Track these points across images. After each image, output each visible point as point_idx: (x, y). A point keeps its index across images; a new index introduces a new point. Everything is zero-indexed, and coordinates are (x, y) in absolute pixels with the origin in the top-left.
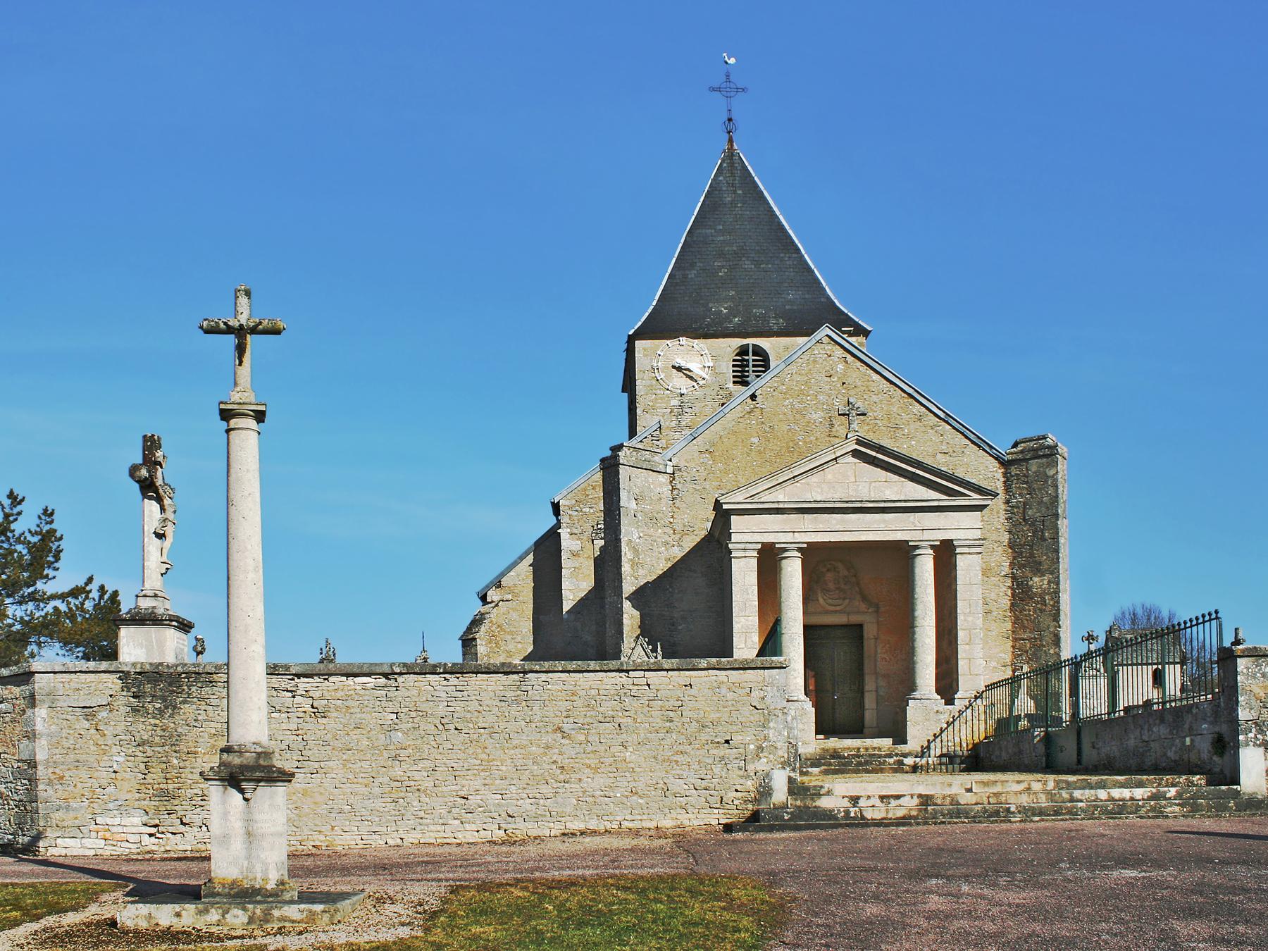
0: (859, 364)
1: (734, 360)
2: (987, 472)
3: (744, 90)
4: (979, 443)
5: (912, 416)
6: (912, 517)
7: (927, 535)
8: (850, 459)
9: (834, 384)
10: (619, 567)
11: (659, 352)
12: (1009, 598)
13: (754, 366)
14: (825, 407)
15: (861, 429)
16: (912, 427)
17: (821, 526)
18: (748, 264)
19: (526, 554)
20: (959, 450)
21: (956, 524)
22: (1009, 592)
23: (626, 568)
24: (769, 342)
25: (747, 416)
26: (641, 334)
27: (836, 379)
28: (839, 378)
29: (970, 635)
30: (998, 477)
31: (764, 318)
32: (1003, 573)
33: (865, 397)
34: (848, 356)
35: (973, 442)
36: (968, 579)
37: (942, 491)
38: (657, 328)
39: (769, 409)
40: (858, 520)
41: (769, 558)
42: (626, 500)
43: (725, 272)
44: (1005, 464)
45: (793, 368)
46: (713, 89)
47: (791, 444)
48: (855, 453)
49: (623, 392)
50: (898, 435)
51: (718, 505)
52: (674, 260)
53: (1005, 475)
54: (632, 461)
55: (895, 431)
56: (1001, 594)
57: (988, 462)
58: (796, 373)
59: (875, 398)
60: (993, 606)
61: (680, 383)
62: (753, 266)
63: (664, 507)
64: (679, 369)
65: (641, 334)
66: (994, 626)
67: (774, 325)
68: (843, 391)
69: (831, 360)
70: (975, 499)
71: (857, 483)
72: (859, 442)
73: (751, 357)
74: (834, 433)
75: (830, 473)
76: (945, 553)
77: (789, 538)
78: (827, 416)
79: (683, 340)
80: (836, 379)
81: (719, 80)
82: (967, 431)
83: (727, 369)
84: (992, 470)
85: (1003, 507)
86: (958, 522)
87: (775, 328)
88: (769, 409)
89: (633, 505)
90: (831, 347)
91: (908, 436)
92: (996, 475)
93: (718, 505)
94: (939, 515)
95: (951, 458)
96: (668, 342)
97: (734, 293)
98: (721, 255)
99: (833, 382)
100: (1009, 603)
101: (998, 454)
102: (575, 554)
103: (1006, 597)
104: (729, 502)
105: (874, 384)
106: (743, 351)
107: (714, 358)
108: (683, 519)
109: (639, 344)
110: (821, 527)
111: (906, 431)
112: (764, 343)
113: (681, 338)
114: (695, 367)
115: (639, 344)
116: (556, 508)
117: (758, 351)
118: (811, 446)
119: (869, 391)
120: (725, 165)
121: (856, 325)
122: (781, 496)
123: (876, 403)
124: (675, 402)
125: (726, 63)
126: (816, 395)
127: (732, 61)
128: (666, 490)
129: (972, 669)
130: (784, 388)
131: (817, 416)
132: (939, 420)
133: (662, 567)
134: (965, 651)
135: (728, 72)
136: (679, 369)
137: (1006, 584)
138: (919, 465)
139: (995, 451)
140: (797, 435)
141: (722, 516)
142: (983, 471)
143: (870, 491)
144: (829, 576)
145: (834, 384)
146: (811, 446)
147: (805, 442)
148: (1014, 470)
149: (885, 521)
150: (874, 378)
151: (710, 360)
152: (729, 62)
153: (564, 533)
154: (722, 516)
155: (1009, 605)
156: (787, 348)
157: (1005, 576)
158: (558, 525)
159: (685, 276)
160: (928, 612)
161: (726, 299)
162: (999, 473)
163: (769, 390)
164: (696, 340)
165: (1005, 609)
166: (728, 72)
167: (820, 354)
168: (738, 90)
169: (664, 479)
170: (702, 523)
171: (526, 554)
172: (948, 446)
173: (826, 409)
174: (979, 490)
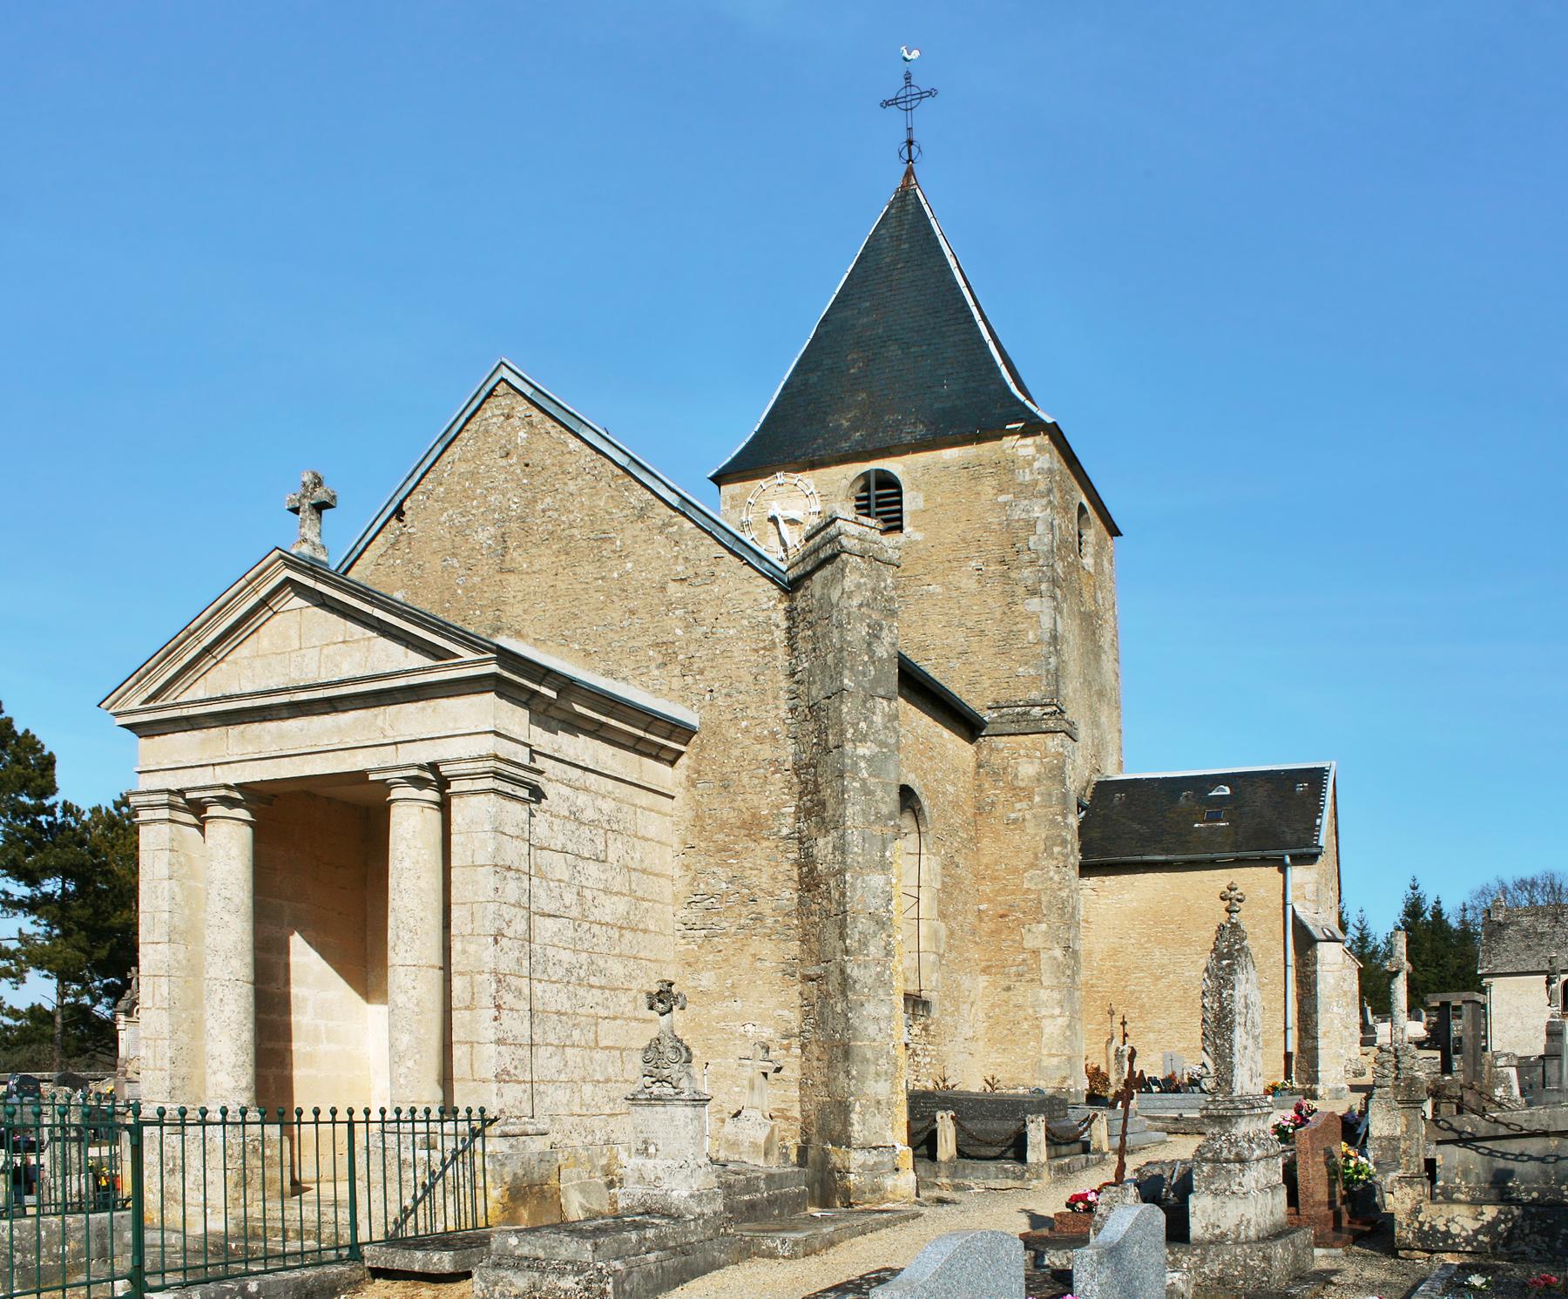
0: (549, 423)
1: (858, 499)
3: (931, 93)
5: (629, 512)
6: (381, 717)
9: (512, 469)
11: (749, 499)
12: (795, 886)
13: (878, 505)
14: (496, 516)
16: (628, 533)
17: (250, 749)
20: (704, 569)
21: (451, 725)
22: (795, 874)
24: (898, 462)
25: (390, 552)
27: (515, 459)
28: (520, 456)
29: (472, 985)
30: (778, 621)
32: (785, 831)
33: (557, 486)
34: (535, 412)
35: (732, 552)
36: (469, 853)
37: (428, 652)
39: (420, 534)
40: (301, 730)
43: (859, 367)
46: (885, 104)
47: (447, 595)
50: (604, 553)
52: (797, 359)
53: (790, 614)
55: (600, 547)
56: (780, 877)
57: (760, 590)
58: (459, 459)
59: (572, 487)
60: (765, 906)
62: (899, 352)
66: (766, 948)
68: (525, 481)
69: (509, 424)
71: (303, 652)
72: (292, 563)
74: (507, 565)
78: (499, 533)
79: (781, 477)
80: (515, 459)
81: (894, 86)
82: (719, 529)
84: (765, 607)
85: (785, 684)
86: (455, 720)
87: (907, 439)
88: (420, 534)
92: (774, 616)
94: (423, 709)
95: (692, 589)
96: (762, 482)
97: (864, 395)
99: (511, 466)
100: (795, 896)
101: (773, 569)
103: (790, 884)
105: (573, 459)
107: (824, 498)
110: (250, 750)
111: (618, 543)
113: (778, 474)
118: (474, 594)
119: (563, 472)
120: (893, 211)
123: (572, 494)
125: (905, 59)
126: (486, 496)
129: (475, 1066)
130: (442, 489)
132: (673, 514)
134: (463, 1025)
135: (908, 73)
137: (789, 855)
139: (767, 565)
140: (456, 576)
142: (749, 611)
143: (319, 667)
145: (512, 469)
146: (474, 594)
147: (465, 588)
149: (339, 729)
150: (571, 446)
151: (818, 501)
152: (909, 57)
155: (796, 900)
156: (927, 468)
157: (788, 837)
160: (401, 934)
163: (421, 498)
164: (799, 475)
165: (788, 909)
166: (908, 73)
167: (494, 416)
172: (688, 565)
173: (498, 520)
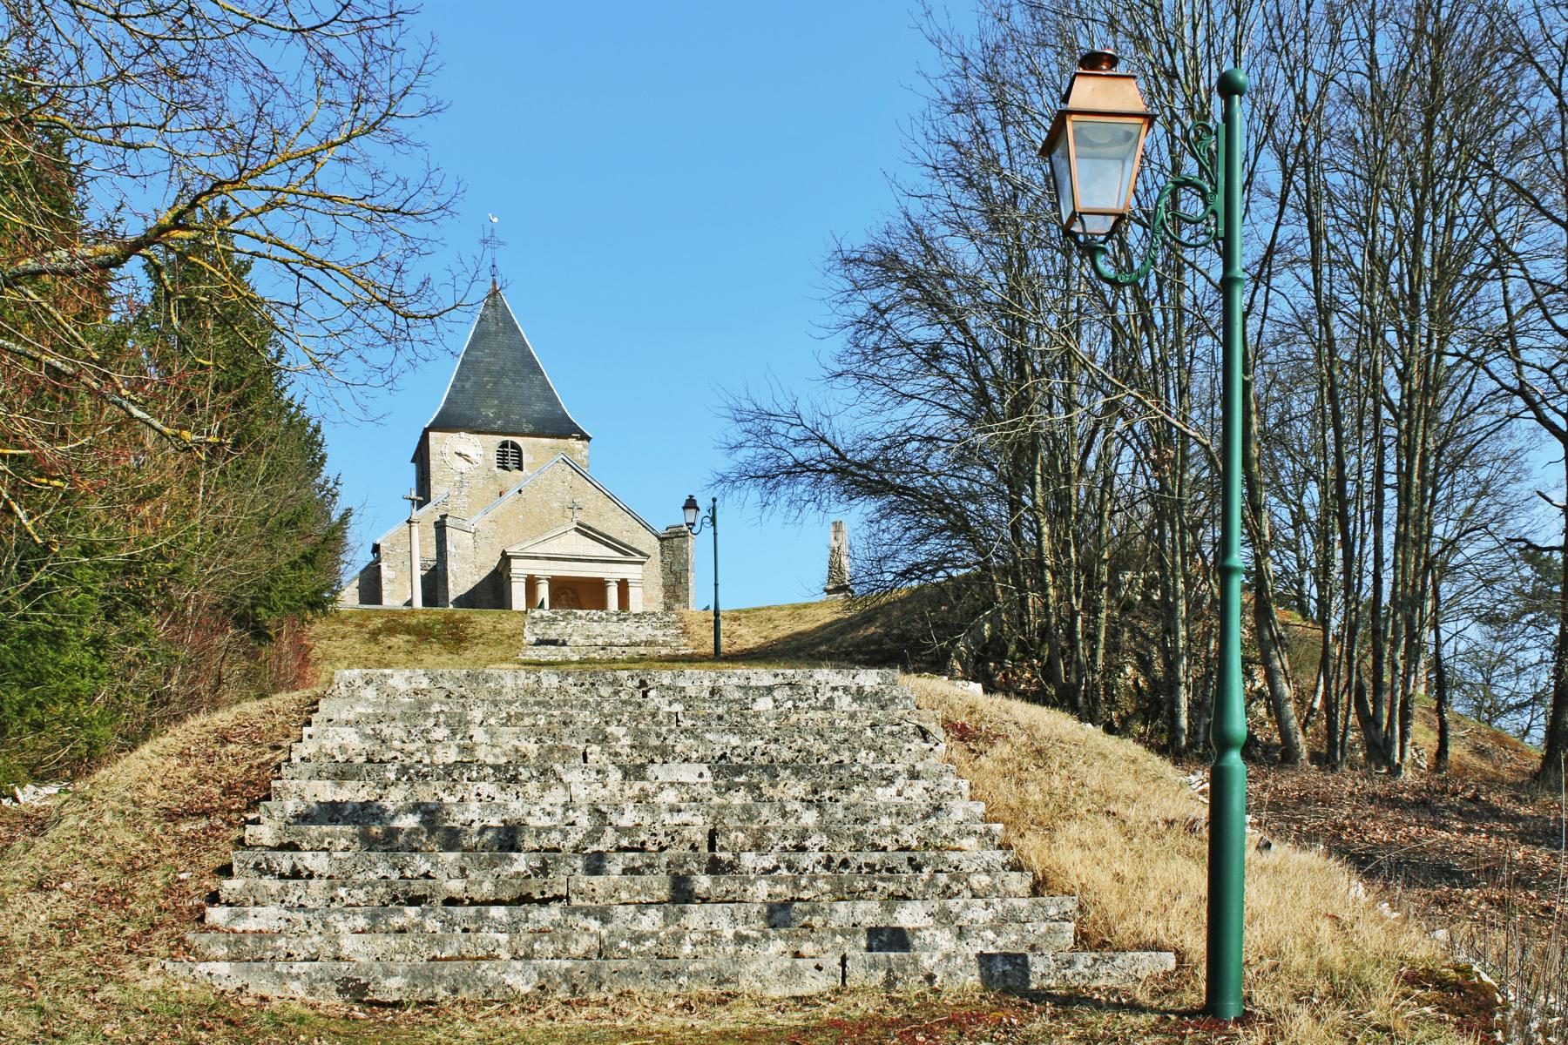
2: (649, 544)
4: (646, 527)
7: (614, 576)
8: (573, 532)
10: (446, 585)
15: (580, 516)
18: (507, 381)
19: (355, 578)
23: (450, 586)
26: (435, 427)
31: (519, 422)
38: (447, 422)
41: (531, 583)
42: (450, 547)
44: (661, 539)
45: (543, 476)
48: (576, 529)
49: (413, 461)
51: (504, 553)
54: (453, 524)
61: (461, 464)
63: (470, 552)
64: (460, 454)
65: (433, 427)
67: (528, 428)
70: (638, 558)
73: (510, 450)
75: (564, 538)
76: (623, 586)
77: (542, 572)
79: (463, 434)
83: (493, 457)
87: (527, 430)
89: (453, 550)
90: (564, 465)
91: (606, 520)
93: (504, 553)
98: (489, 372)
102: (391, 581)
104: (510, 551)
106: (504, 445)
108: (481, 559)
109: (432, 435)
112: (518, 440)
114: (472, 453)
115: (432, 435)
116: (376, 548)
117: (514, 446)
121: (582, 432)
122: (538, 550)
124: (457, 478)
127: (495, 220)
128: (471, 542)
131: (556, 505)
133: (469, 587)
136: (460, 454)
138: (609, 538)
141: (506, 559)
144: (563, 597)
148: (665, 543)
153: (383, 565)
154: (506, 559)
158: (378, 560)
159: (463, 387)
161: (493, 406)
162: (656, 543)
168: (500, 243)
169: (470, 535)
170: (493, 562)
171: (355, 578)
174: (641, 553)
